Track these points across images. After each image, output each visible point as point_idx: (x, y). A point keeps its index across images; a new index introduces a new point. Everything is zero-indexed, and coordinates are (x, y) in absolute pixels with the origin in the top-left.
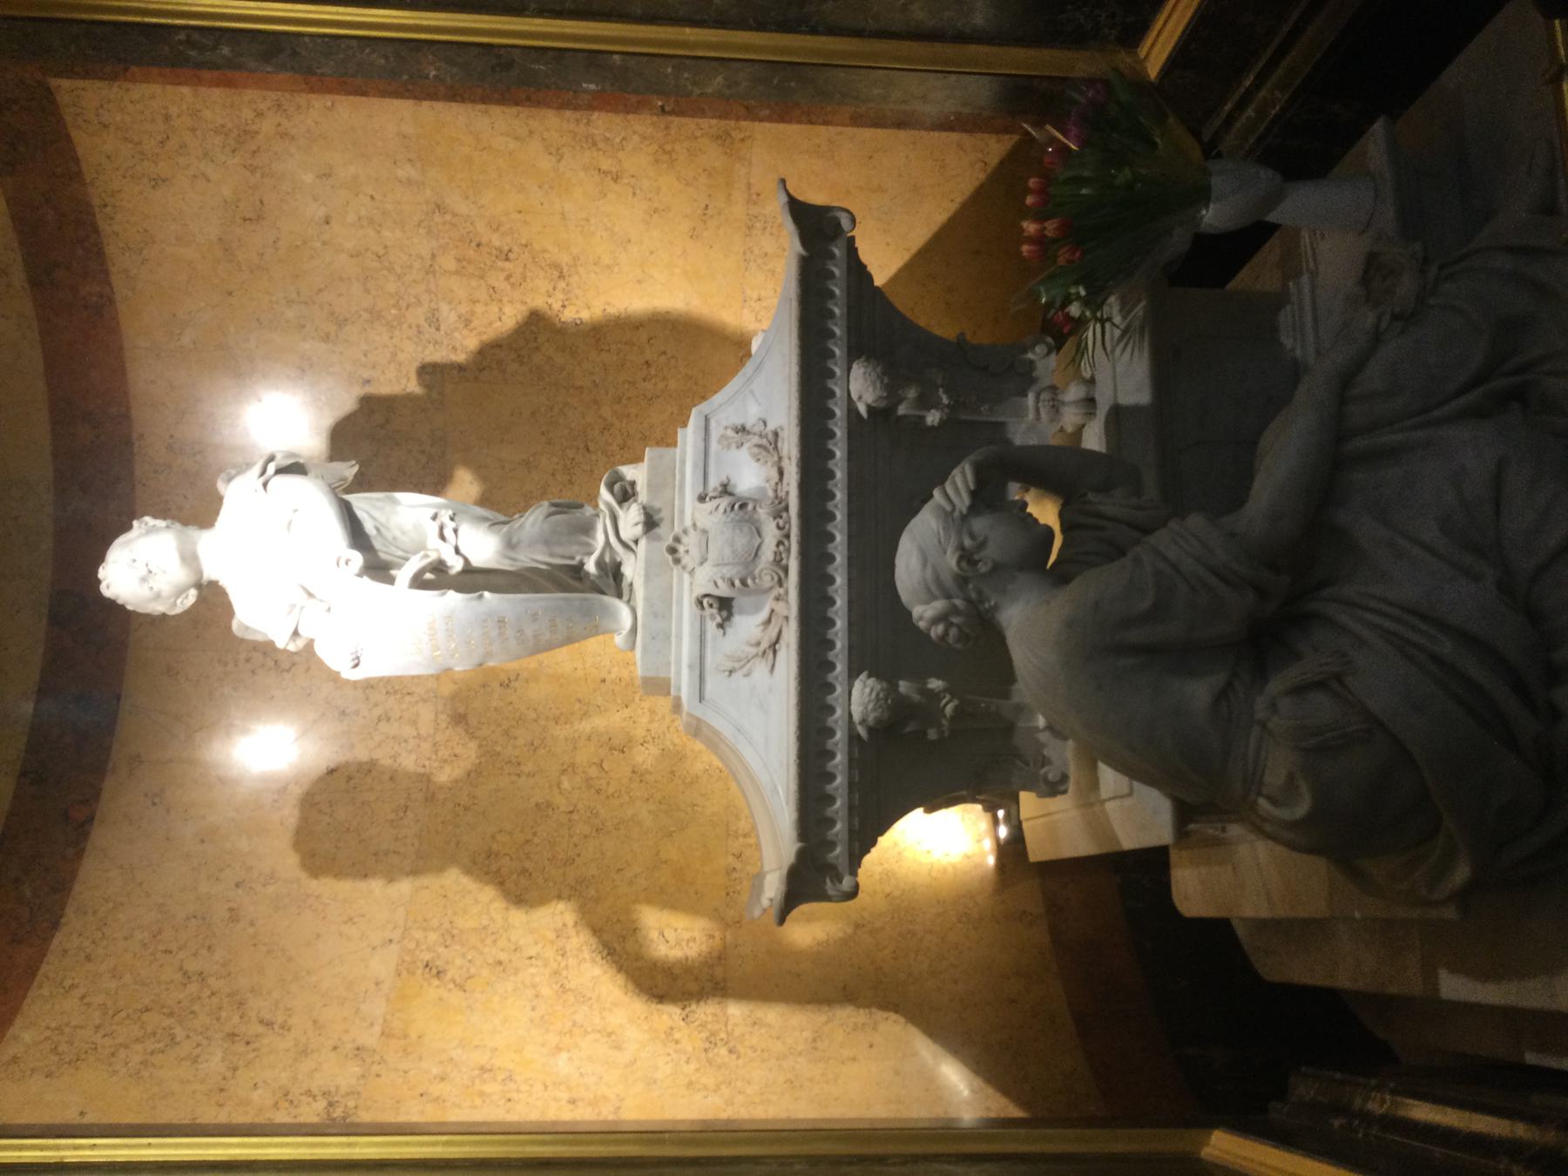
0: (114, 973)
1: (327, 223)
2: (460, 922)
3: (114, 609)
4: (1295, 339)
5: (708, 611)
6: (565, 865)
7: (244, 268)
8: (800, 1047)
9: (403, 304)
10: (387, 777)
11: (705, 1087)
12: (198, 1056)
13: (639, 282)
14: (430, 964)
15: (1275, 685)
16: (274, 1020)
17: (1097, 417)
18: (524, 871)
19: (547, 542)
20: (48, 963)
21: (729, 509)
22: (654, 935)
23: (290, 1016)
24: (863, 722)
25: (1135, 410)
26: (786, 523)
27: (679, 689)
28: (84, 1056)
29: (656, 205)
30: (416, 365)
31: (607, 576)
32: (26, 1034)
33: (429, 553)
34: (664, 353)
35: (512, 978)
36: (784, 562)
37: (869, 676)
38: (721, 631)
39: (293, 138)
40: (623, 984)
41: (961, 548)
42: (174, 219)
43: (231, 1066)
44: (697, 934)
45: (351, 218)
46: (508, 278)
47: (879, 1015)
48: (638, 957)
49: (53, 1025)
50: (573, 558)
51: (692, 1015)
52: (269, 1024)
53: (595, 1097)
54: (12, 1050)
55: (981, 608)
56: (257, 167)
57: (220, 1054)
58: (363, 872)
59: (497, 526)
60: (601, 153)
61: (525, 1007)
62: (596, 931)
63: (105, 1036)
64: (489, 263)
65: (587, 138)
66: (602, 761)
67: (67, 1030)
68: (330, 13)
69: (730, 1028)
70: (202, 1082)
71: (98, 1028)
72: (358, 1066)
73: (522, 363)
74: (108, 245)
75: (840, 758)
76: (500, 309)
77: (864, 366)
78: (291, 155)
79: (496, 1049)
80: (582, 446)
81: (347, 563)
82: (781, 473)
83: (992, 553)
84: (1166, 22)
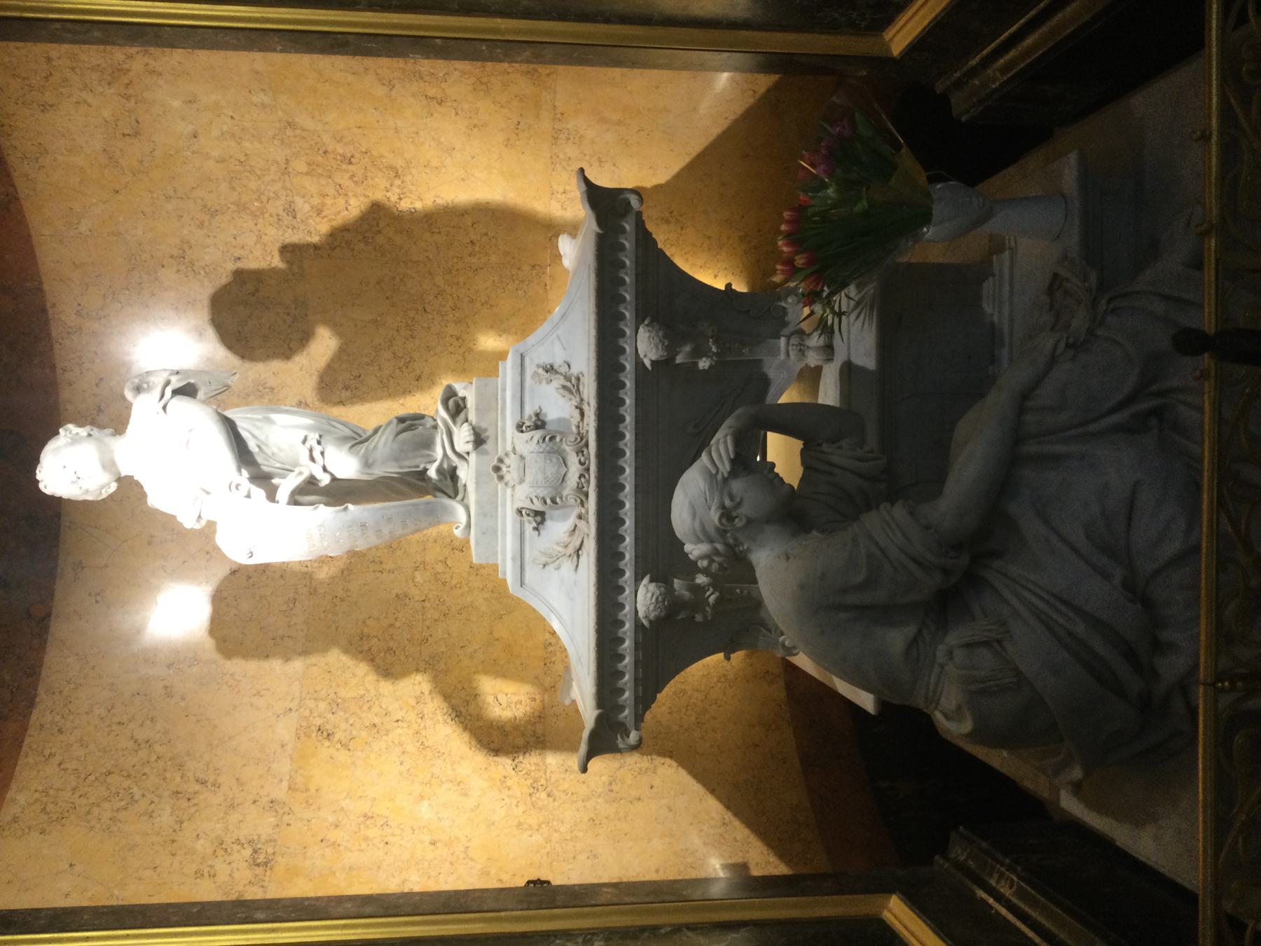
0: (82, 743)
1: (195, 137)
2: (343, 693)
3: (56, 503)
4: (994, 308)
5: (526, 518)
6: (420, 645)
7: (126, 172)
8: (600, 790)
9: (264, 198)
10: (278, 575)
11: (531, 828)
12: (153, 812)
13: (463, 180)
14: (321, 728)
15: (953, 638)
16: (207, 779)
17: (834, 363)
18: (390, 649)
19: (397, 460)
20: (30, 736)
21: (541, 441)
22: (490, 699)
23: (219, 775)
24: (646, 617)
25: (862, 370)
26: (586, 459)
27: (505, 573)
28: (66, 814)
29: (475, 121)
30: (278, 245)
31: (446, 479)
32: (20, 798)
33: (302, 469)
34: (486, 234)
35: (384, 738)
36: (585, 489)
37: (651, 581)
38: (537, 532)
39: (160, 74)
40: (468, 741)
41: (723, 507)
42: (63, 136)
43: (178, 819)
44: (523, 698)
45: (215, 133)
46: (352, 177)
47: (659, 760)
48: (479, 718)
49: (40, 788)
50: (418, 467)
51: (519, 765)
52: (204, 783)
53: (450, 838)
54: (11, 810)
55: (737, 549)
56: (131, 96)
57: (168, 811)
58: (264, 653)
59: (355, 447)
60: (427, 84)
61: (395, 762)
62: (447, 697)
63: (81, 796)
64: (335, 166)
65: (414, 73)
66: (446, 558)
67: (52, 792)
68: (185, 9)
69: (548, 775)
70: (158, 834)
71: (74, 789)
72: (274, 817)
73: (367, 243)
74: (8, 155)
75: (628, 644)
76: (347, 202)
77: (649, 331)
78: (160, 86)
79: (375, 799)
80: (420, 308)
81: (237, 488)
82: (582, 414)
83: (745, 510)
84: (913, 16)
